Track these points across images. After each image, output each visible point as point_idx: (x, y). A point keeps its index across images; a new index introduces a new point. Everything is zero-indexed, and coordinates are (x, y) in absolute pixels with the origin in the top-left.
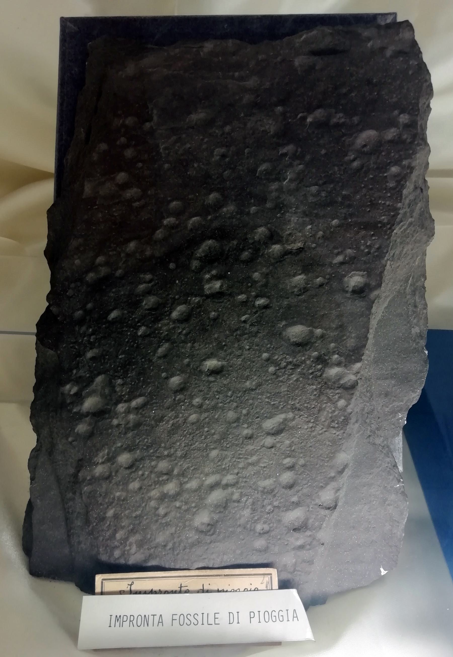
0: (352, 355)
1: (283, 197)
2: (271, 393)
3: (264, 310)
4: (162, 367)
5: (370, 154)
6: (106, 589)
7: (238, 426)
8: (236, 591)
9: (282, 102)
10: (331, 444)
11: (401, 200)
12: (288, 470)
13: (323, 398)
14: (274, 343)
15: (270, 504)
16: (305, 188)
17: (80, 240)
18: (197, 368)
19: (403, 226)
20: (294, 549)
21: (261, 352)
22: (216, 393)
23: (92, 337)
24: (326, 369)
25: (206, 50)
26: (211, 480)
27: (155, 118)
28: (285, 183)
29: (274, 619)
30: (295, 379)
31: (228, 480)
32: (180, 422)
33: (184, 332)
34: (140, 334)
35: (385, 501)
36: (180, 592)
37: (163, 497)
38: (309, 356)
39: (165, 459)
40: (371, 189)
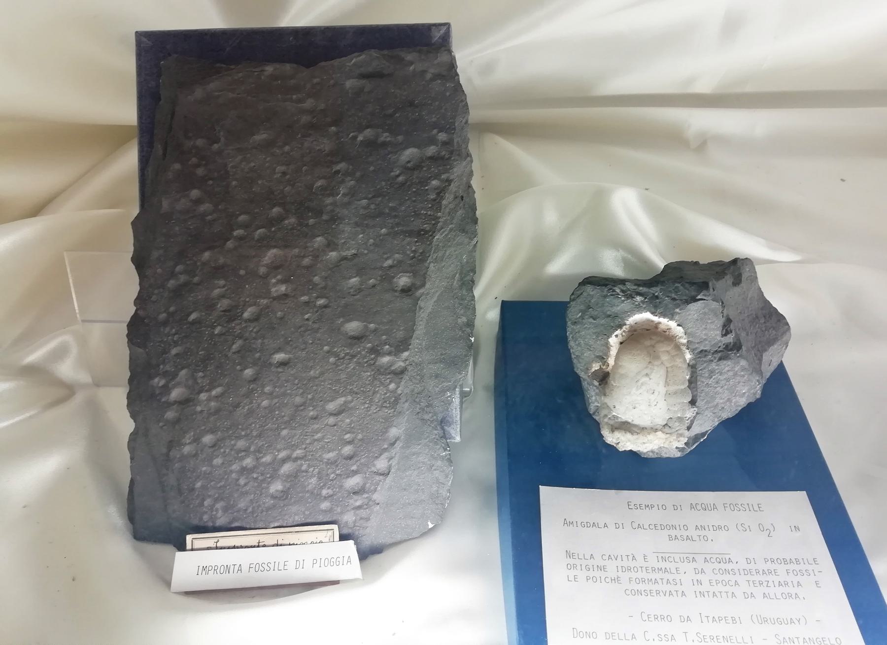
0: (401, 346)
1: (337, 210)
2: (332, 380)
3: (324, 309)
4: (237, 361)
5: (413, 169)
6: (195, 547)
7: (305, 408)
8: (304, 544)
9: (335, 123)
10: (384, 421)
11: (440, 210)
12: (348, 444)
13: (377, 383)
14: (333, 338)
15: (334, 473)
16: (356, 202)
17: (161, 252)
18: (267, 360)
19: (443, 232)
20: (353, 509)
21: (322, 346)
22: (285, 382)
23: (176, 336)
24: (378, 358)
25: (266, 73)
26: (282, 455)
27: (223, 139)
28: (338, 198)
29: (332, 564)
30: (352, 367)
31: (298, 454)
32: (254, 408)
33: (255, 330)
34: (216, 333)
35: (431, 467)
36: (258, 546)
37: (244, 470)
38: (364, 347)
39: (242, 439)
40: (414, 201)
